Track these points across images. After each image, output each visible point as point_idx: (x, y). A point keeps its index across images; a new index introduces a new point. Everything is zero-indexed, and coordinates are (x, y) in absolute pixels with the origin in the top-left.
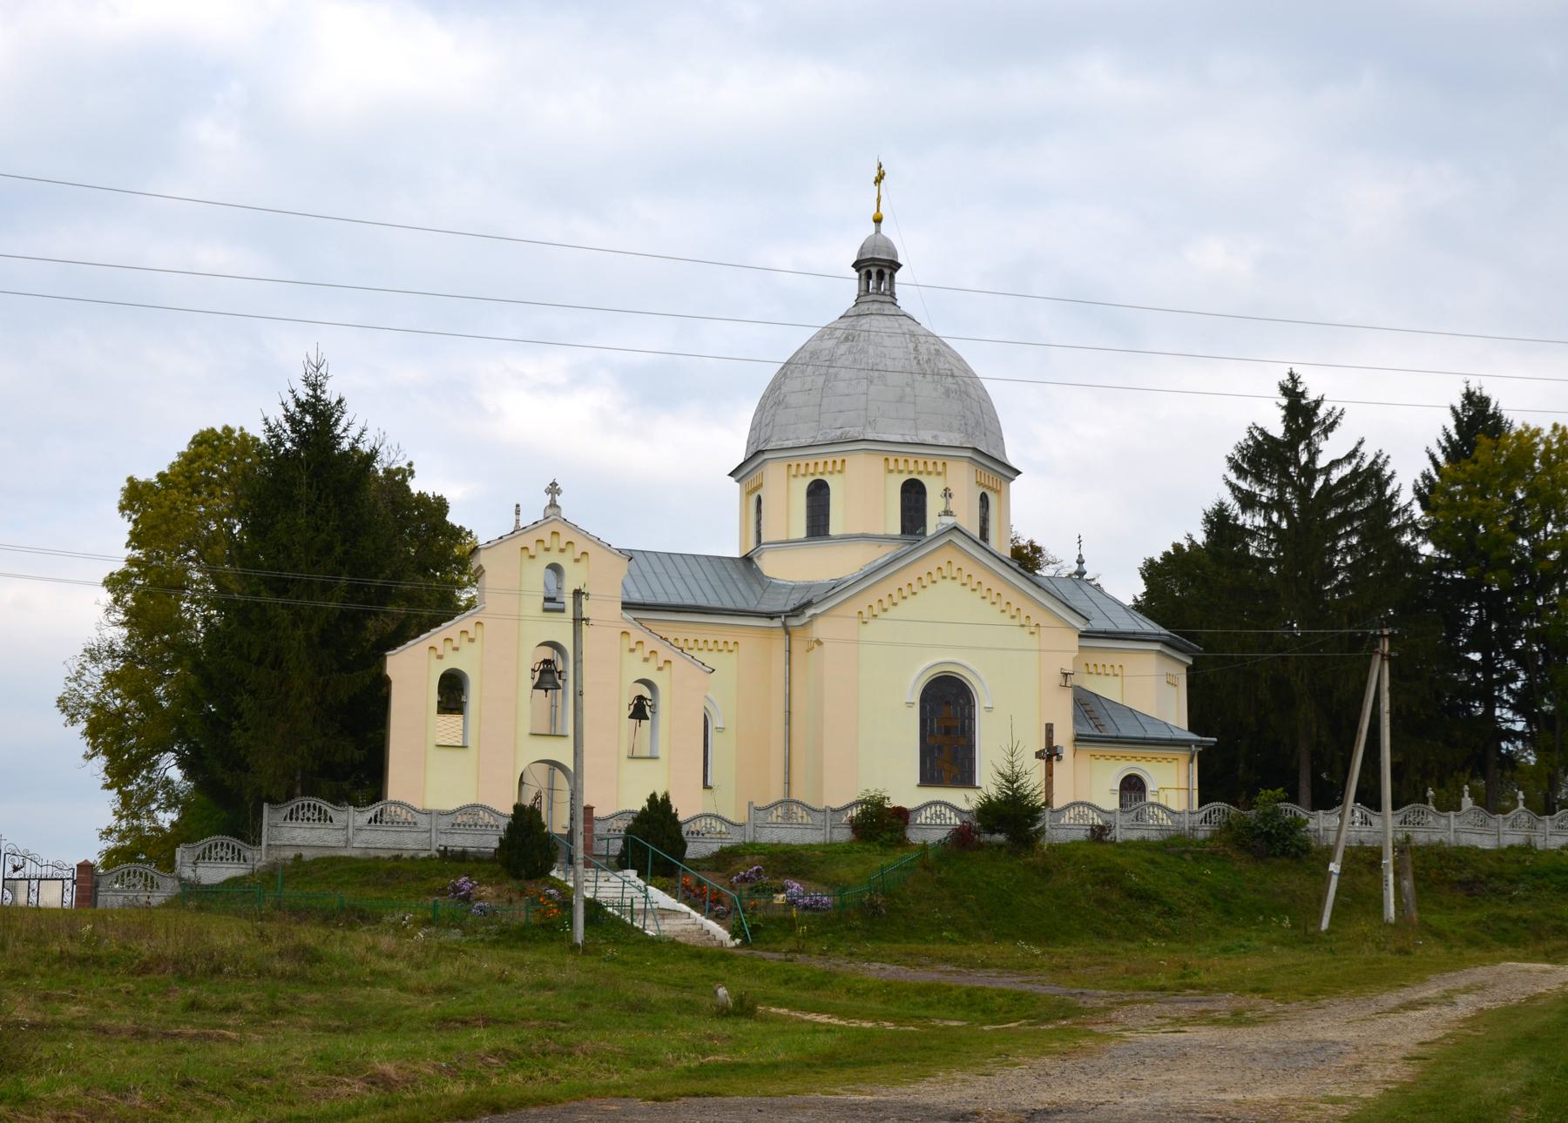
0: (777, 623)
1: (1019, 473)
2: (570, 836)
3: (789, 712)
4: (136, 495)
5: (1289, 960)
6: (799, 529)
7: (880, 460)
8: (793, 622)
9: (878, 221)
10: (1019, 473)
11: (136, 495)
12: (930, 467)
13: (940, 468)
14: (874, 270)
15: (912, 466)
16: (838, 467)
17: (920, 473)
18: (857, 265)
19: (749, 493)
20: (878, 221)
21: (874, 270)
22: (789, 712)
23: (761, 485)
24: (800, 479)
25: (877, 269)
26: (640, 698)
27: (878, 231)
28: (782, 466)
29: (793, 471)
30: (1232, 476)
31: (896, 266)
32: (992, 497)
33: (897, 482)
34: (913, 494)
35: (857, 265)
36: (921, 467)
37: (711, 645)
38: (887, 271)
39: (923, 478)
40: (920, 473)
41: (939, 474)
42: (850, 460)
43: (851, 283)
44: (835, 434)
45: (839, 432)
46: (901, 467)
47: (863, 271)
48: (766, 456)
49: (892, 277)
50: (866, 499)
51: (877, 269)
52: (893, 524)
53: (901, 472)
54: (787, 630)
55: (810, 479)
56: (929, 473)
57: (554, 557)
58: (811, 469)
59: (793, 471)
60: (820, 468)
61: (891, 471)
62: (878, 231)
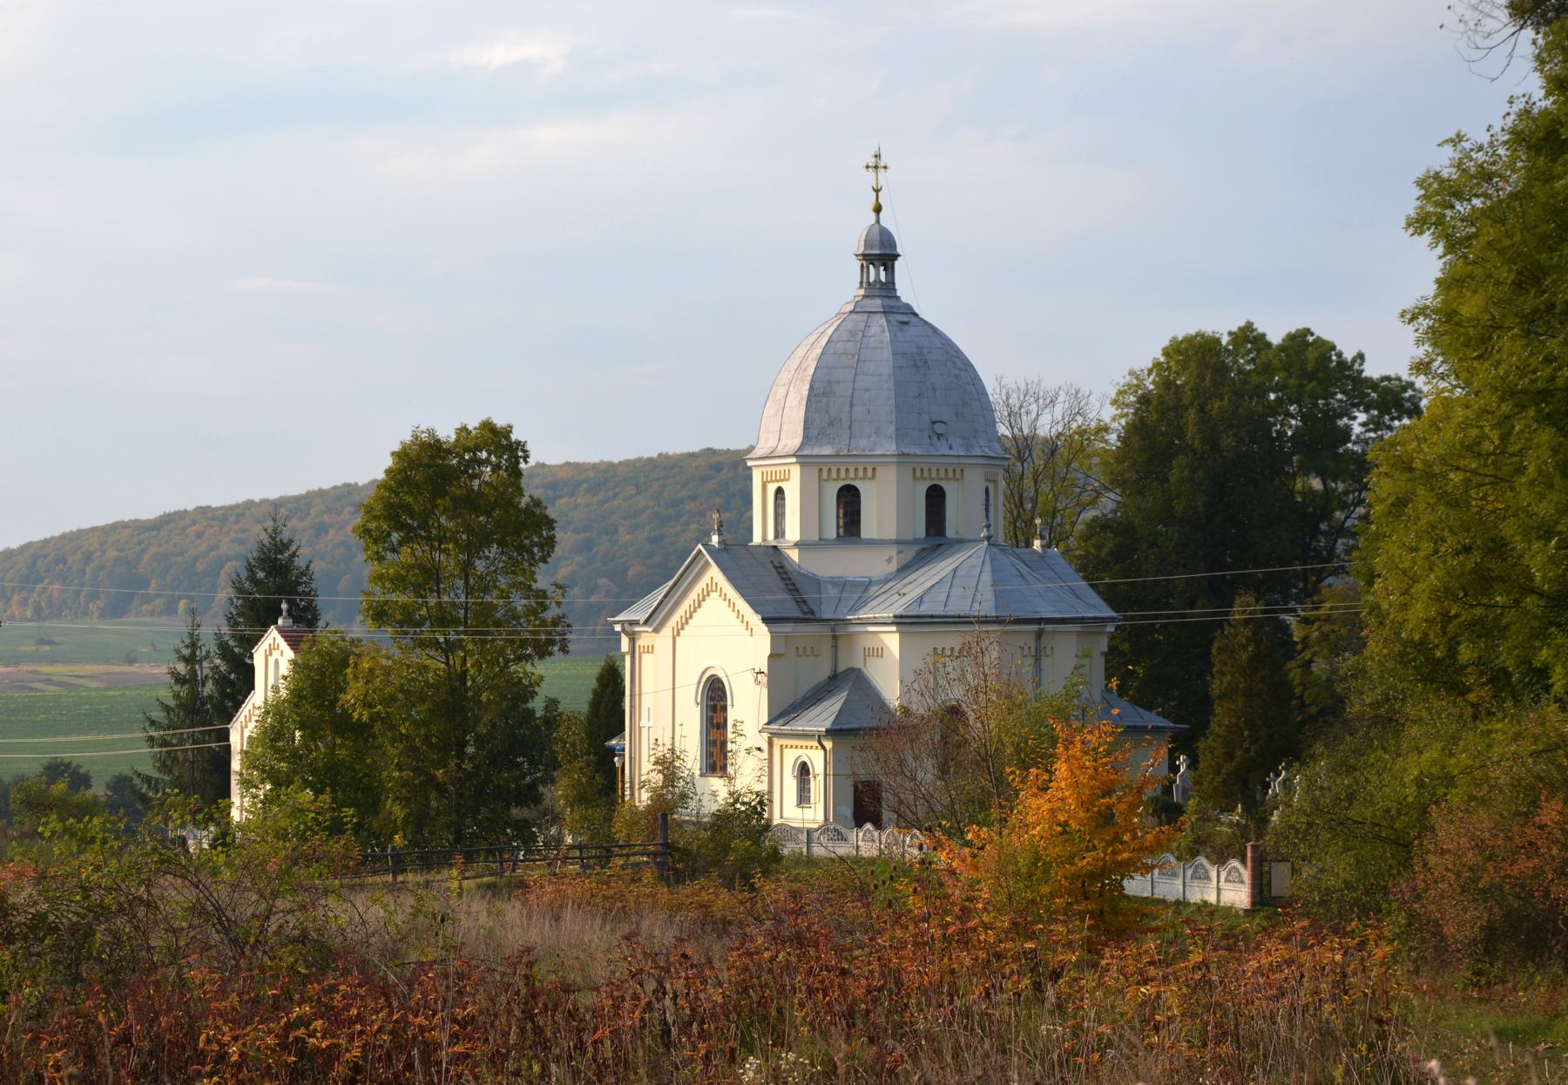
11: (1249, 327)
16: (870, 474)
27: (878, 221)
29: (825, 475)
33: (832, 489)
34: (935, 497)
39: (943, 484)
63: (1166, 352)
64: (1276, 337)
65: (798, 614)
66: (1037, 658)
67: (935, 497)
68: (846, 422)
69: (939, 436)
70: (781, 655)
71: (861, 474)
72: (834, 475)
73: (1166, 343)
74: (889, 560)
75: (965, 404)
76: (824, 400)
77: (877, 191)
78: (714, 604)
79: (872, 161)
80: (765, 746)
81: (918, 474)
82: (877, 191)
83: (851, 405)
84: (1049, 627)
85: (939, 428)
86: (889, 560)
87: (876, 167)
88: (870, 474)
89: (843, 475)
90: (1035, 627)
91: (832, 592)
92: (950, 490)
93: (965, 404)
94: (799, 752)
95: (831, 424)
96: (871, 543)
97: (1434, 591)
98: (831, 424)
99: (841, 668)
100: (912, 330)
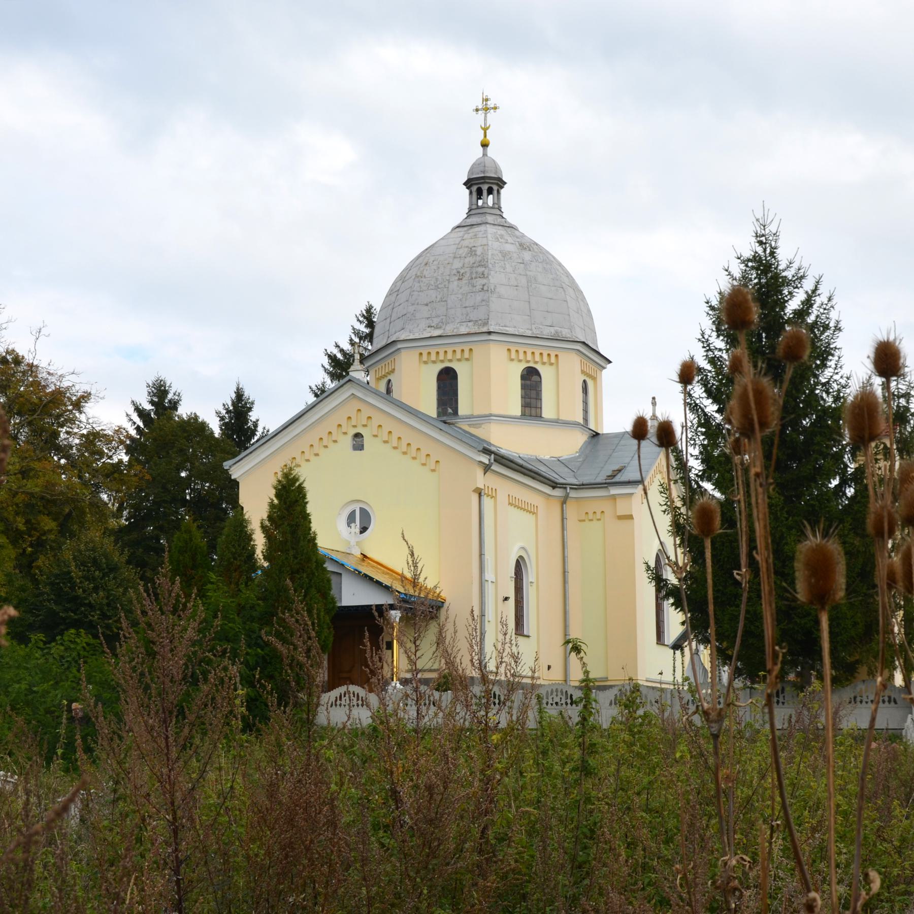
0: (558, 492)
3: (565, 572)
6: (516, 408)
8: (573, 494)
9: (485, 145)
10: (610, 362)
12: (545, 359)
13: (553, 359)
14: (485, 187)
15: (529, 357)
16: (466, 355)
17: (450, 361)
18: (469, 184)
20: (485, 145)
21: (485, 187)
22: (565, 572)
23: (393, 371)
24: (431, 365)
25: (484, 185)
26: (521, 557)
27: (485, 155)
28: (414, 354)
29: (425, 358)
31: (501, 183)
32: (590, 383)
33: (518, 369)
35: (469, 184)
36: (537, 358)
37: (591, 516)
38: (495, 188)
39: (539, 367)
40: (536, 362)
42: (563, 356)
43: (460, 200)
44: (547, 332)
45: (552, 330)
46: (521, 356)
47: (474, 188)
48: (399, 346)
49: (498, 192)
51: (484, 185)
53: (520, 361)
55: (441, 366)
56: (544, 363)
57: (360, 430)
58: (441, 357)
59: (425, 358)
60: (450, 356)
61: (512, 360)
62: (485, 155)
71: (458, 356)
72: (433, 357)
77: (485, 130)
81: (514, 355)
82: (485, 130)
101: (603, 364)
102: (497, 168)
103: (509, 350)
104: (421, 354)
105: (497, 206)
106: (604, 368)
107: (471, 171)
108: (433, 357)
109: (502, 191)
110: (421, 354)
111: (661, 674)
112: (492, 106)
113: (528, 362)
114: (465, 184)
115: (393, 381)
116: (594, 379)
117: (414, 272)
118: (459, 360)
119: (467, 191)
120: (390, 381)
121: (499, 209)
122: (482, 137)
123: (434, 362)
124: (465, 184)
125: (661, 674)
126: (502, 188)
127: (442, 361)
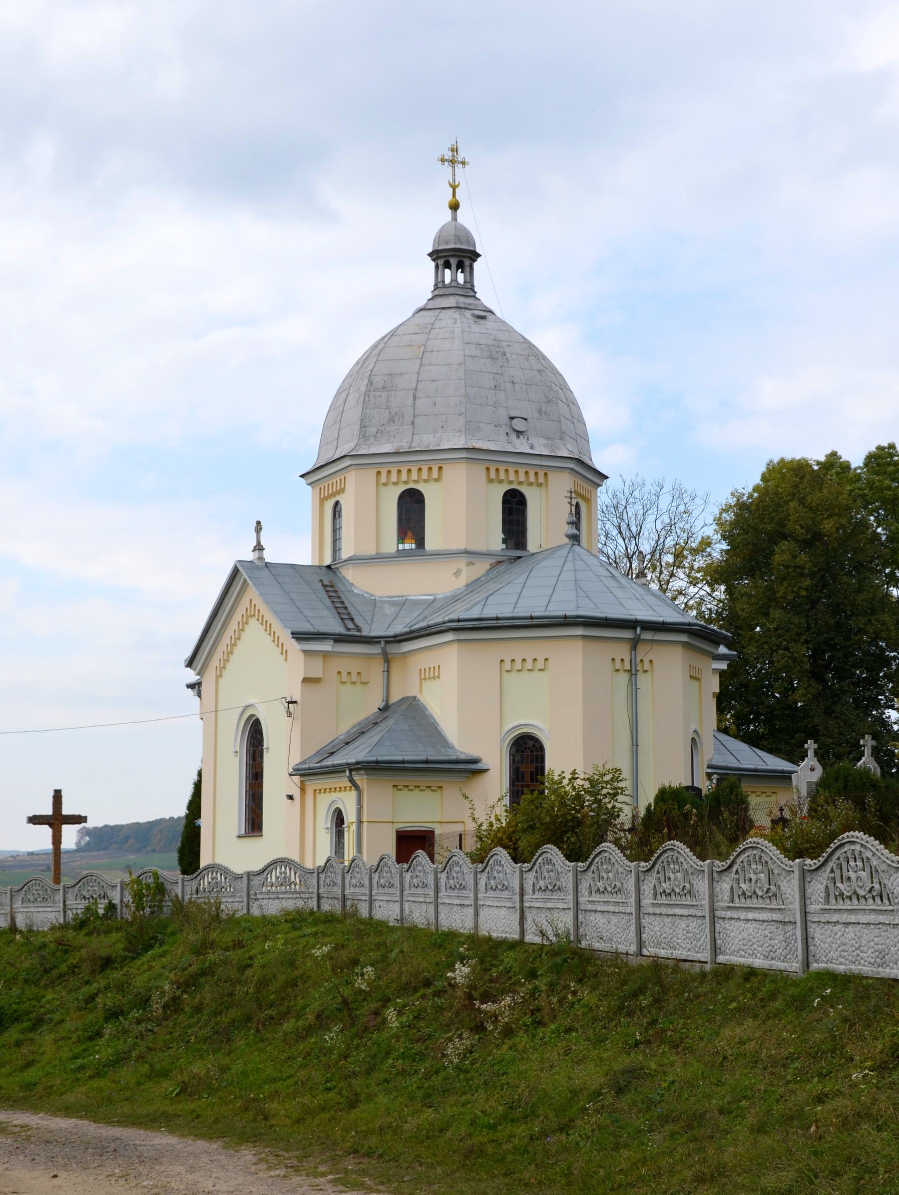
0: (376, 650)
1: (607, 477)
2: (129, 869)
4: (834, 454)
5: (699, 955)
7: (481, 470)
10: (607, 477)
11: (834, 454)
12: (532, 478)
15: (512, 477)
16: (435, 474)
17: (521, 483)
19: (322, 501)
23: (342, 491)
25: (456, 256)
27: (455, 219)
29: (383, 479)
30: (667, 488)
31: (474, 256)
33: (394, 493)
34: (514, 507)
35: (435, 255)
36: (522, 477)
38: (467, 262)
39: (524, 489)
40: (521, 483)
41: (540, 485)
43: (423, 277)
46: (502, 476)
50: (460, 512)
51: (456, 256)
52: (495, 540)
53: (501, 482)
54: (387, 659)
55: (507, 487)
56: (530, 484)
58: (404, 477)
60: (414, 476)
63: (764, 478)
64: (855, 458)
65: (335, 627)
66: (632, 673)
67: (514, 507)
68: (408, 418)
69: (519, 433)
70: (317, 681)
71: (425, 475)
72: (394, 478)
73: (763, 469)
74: (457, 574)
75: (549, 402)
76: (384, 395)
77: (454, 187)
78: (254, 628)
79: (448, 155)
80: (297, 794)
81: (493, 475)
82: (454, 187)
83: (415, 397)
84: (647, 636)
85: (519, 425)
86: (457, 574)
87: (453, 162)
88: (435, 474)
89: (404, 477)
90: (628, 634)
91: (389, 610)
92: (532, 496)
93: (549, 402)
94: (334, 796)
95: (391, 420)
96: (437, 555)
97: (493, 1002)
98: (391, 420)
99: (394, 699)
100: (489, 324)
101: (598, 481)
102: (469, 239)
103: (488, 469)
104: (379, 473)
105: (469, 286)
106: (599, 485)
107: (439, 238)
108: (394, 478)
109: (476, 265)
110: (379, 473)
111: (290, 797)
112: (460, 159)
113: (511, 482)
114: (430, 255)
115: (342, 502)
116: (588, 500)
117: (518, 758)
118: (426, 481)
119: (433, 264)
120: (337, 503)
121: (473, 286)
122: (450, 197)
123: (395, 484)
124: (430, 255)
125: (290, 797)
126: (475, 261)
127: (405, 483)
